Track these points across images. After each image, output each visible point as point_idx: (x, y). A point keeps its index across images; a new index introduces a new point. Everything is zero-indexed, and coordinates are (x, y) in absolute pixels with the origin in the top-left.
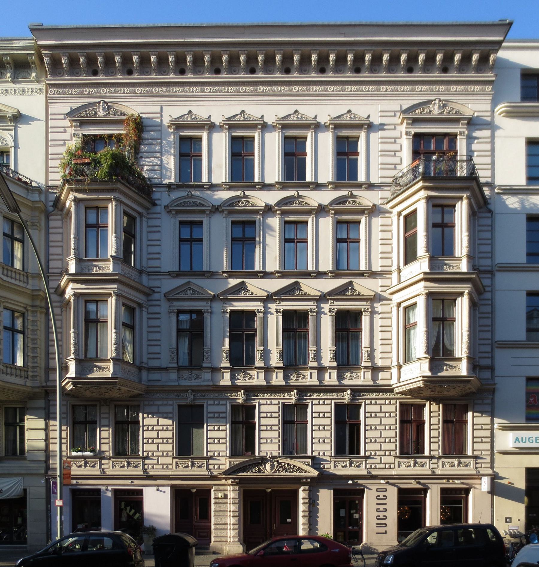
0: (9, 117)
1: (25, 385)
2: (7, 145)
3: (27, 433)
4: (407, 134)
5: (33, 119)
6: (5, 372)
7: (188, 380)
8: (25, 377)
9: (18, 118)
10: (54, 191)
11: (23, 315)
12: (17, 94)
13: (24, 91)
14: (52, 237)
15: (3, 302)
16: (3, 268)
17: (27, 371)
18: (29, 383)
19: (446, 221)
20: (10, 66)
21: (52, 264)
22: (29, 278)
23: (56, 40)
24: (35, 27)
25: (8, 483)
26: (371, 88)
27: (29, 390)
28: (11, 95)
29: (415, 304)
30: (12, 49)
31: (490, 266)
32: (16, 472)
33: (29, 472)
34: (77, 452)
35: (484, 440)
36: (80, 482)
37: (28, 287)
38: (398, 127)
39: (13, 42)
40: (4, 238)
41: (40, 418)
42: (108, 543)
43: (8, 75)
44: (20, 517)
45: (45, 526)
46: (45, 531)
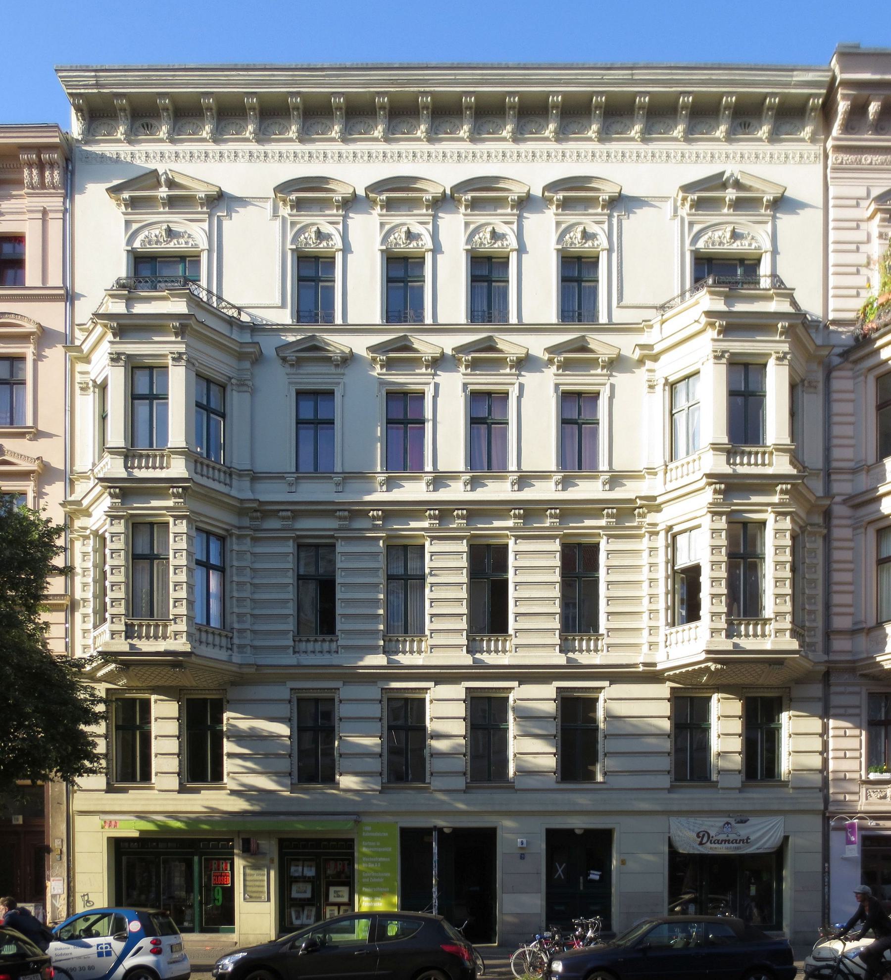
0: (200, 199)
1: (230, 662)
2: (196, 246)
3: (154, 742)
4: (881, 236)
5: (801, 205)
6: (198, 639)
7: (316, 655)
8: (227, 648)
9: (219, 201)
10: (840, 329)
11: (222, 539)
12: (240, 159)
13: (177, 155)
14: (836, 408)
15: (196, 521)
16: (196, 461)
17: (231, 638)
18: (237, 658)
19: (752, 387)
20: (299, 114)
21: (836, 453)
22: (234, 476)
23: (874, 73)
24: (847, 50)
25: (760, 827)
26: (845, 158)
27: (234, 669)
28: (317, 161)
29: (698, 527)
30: (787, 85)
31: (852, 460)
32: (775, 807)
33: (797, 807)
34: (882, 772)
35: (848, 754)
36: (882, 823)
37: (234, 493)
38: (863, 225)
39: (795, 73)
40: (196, 411)
41: (813, 715)
42: (361, 931)
43: (294, 128)
44: (753, 884)
45: (820, 900)
46: (820, 908)
